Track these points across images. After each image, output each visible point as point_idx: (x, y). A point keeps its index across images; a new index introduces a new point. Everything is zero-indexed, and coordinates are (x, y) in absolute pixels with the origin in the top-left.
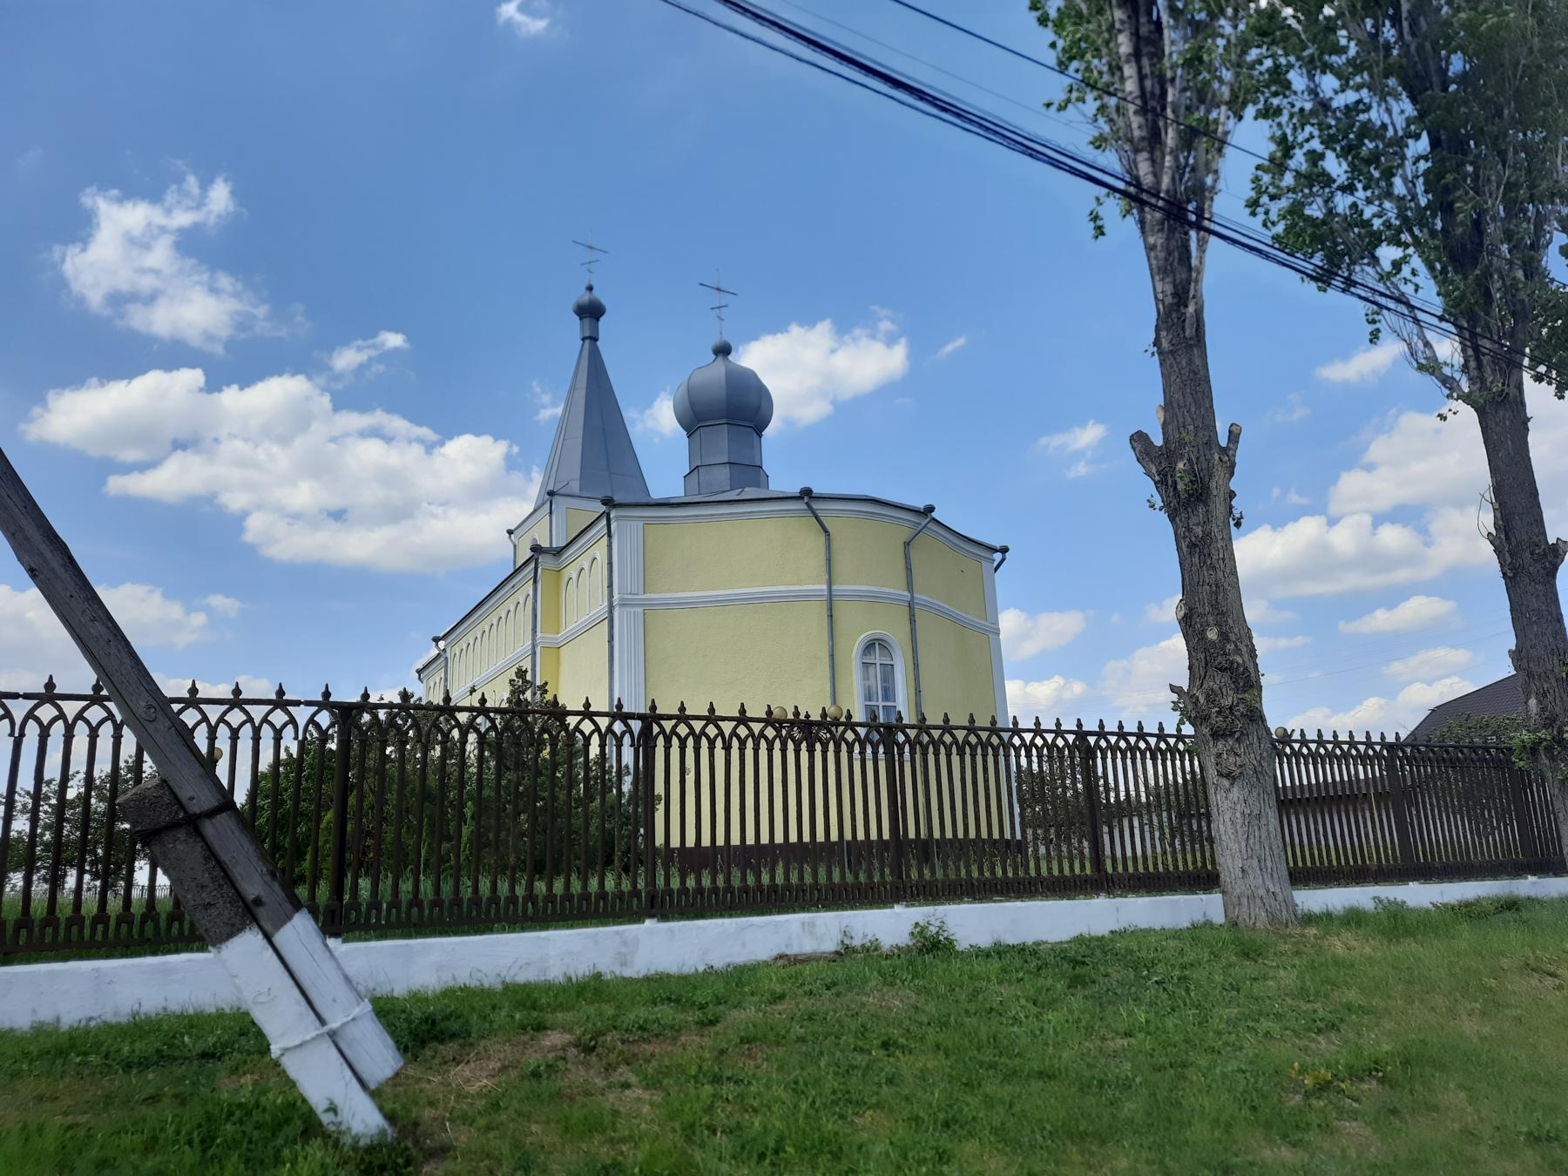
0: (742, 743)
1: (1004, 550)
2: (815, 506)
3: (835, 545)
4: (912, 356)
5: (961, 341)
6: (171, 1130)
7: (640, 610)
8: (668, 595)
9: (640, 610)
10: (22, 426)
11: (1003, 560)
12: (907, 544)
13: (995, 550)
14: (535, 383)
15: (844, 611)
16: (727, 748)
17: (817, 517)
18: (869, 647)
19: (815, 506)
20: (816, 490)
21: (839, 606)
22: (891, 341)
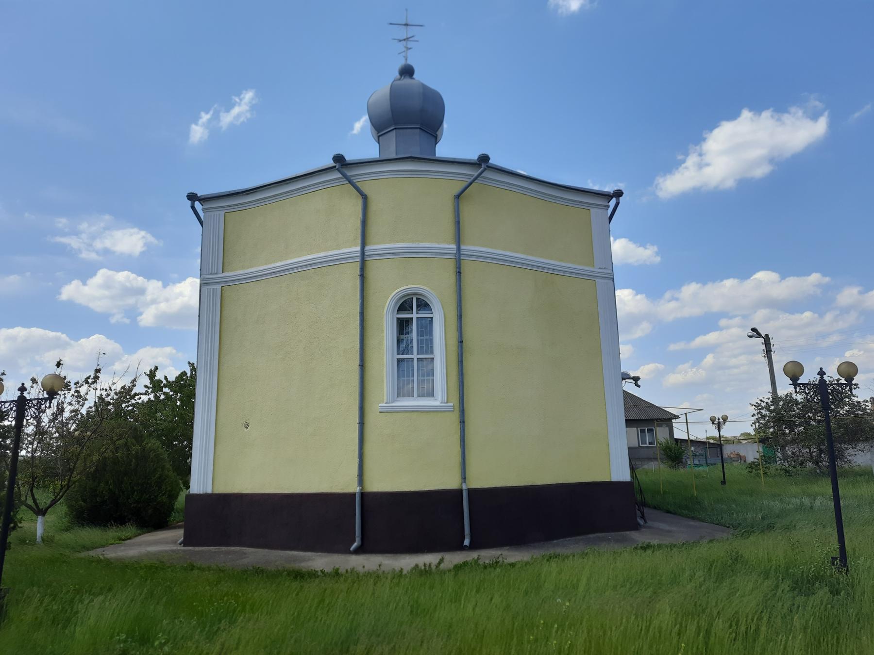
1: (619, 194)
2: (349, 173)
3: (373, 207)
4: (831, 125)
5: (868, 107)
6: (688, 573)
7: (219, 287)
8: (241, 272)
9: (219, 287)
11: (617, 204)
12: (458, 197)
13: (608, 196)
14: (589, 181)
15: (375, 270)
17: (350, 182)
18: (404, 306)
19: (349, 173)
20: (349, 158)
21: (468, 267)
22: (814, 117)
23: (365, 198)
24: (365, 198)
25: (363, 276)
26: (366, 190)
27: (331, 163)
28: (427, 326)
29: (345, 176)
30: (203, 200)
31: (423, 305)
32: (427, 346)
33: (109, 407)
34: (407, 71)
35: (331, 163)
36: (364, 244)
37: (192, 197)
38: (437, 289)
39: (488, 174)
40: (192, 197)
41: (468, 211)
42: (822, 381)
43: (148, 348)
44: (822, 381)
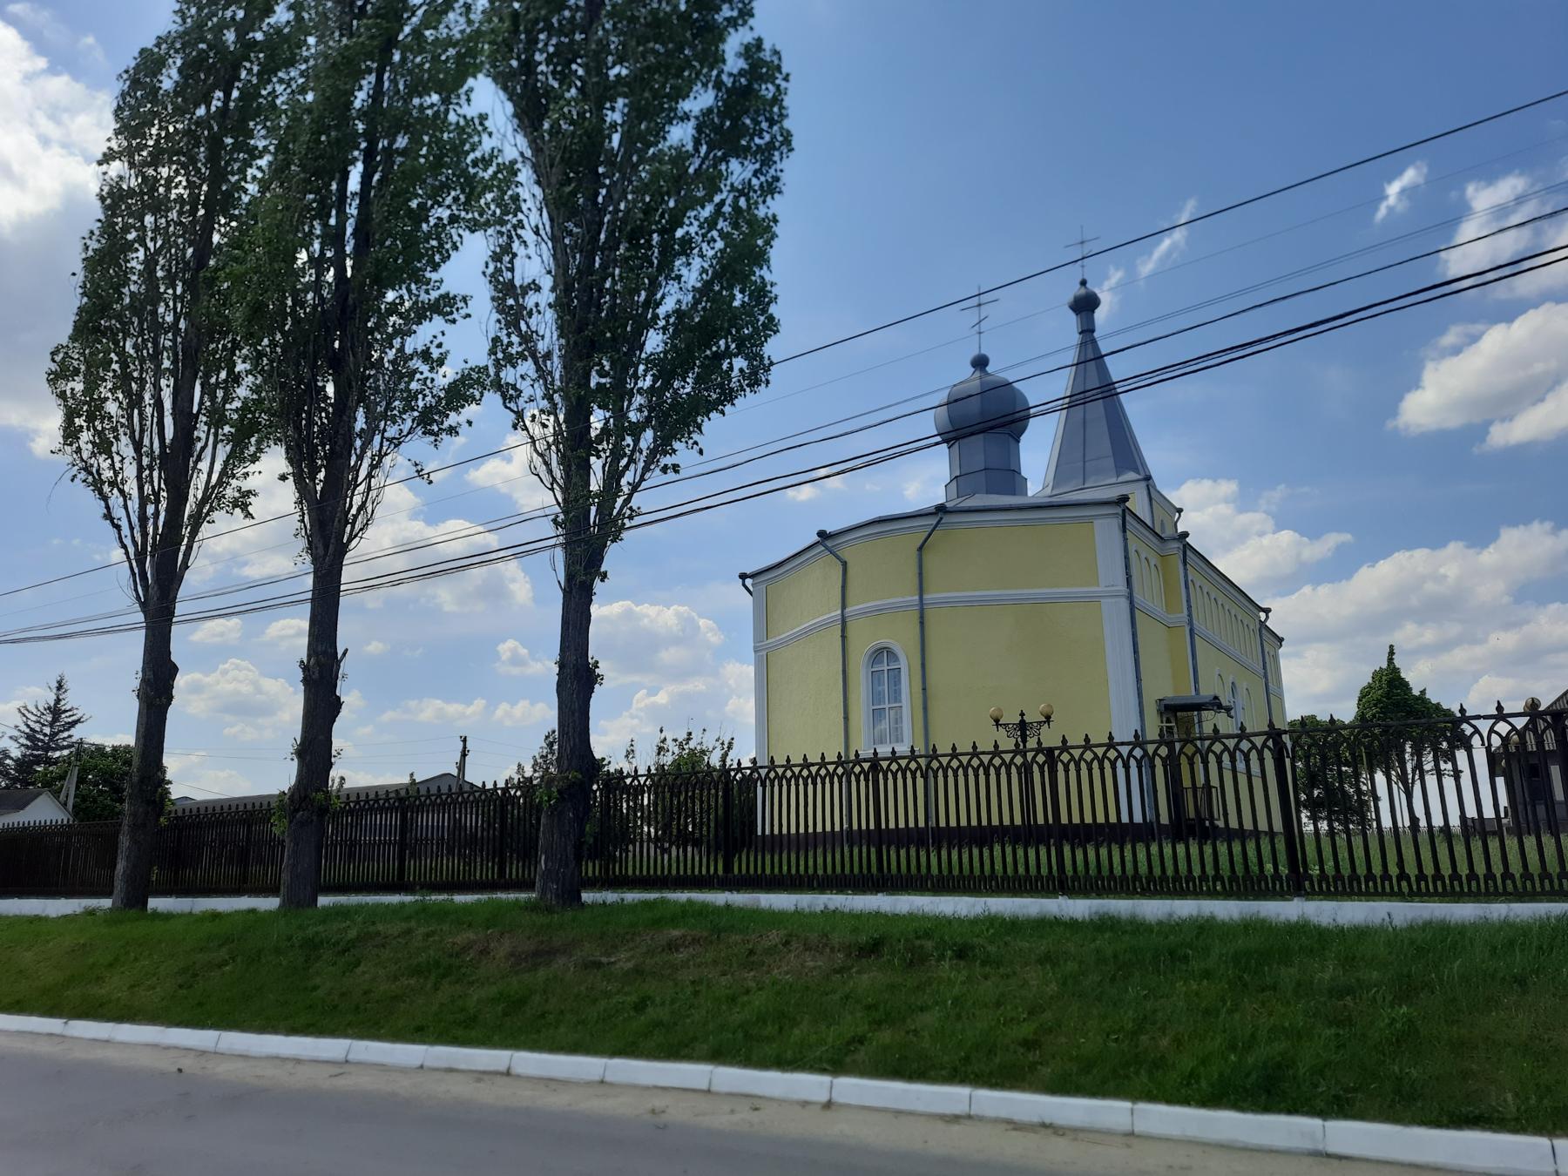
0: (976, 771)
1: (1180, 511)
3: (850, 571)
10: (1390, 424)
12: (920, 549)
16: (1126, 766)
23: (845, 564)
24: (845, 564)
25: (844, 637)
26: (845, 555)
27: (817, 538)
28: (895, 675)
29: (827, 548)
30: (752, 576)
31: (892, 655)
32: (896, 695)
33: (7, 761)
34: (980, 363)
35: (817, 538)
36: (844, 607)
37: (743, 576)
38: (903, 641)
39: (947, 519)
40: (743, 576)
41: (931, 560)
42: (1022, 721)
43: (293, 781)
44: (1022, 721)
